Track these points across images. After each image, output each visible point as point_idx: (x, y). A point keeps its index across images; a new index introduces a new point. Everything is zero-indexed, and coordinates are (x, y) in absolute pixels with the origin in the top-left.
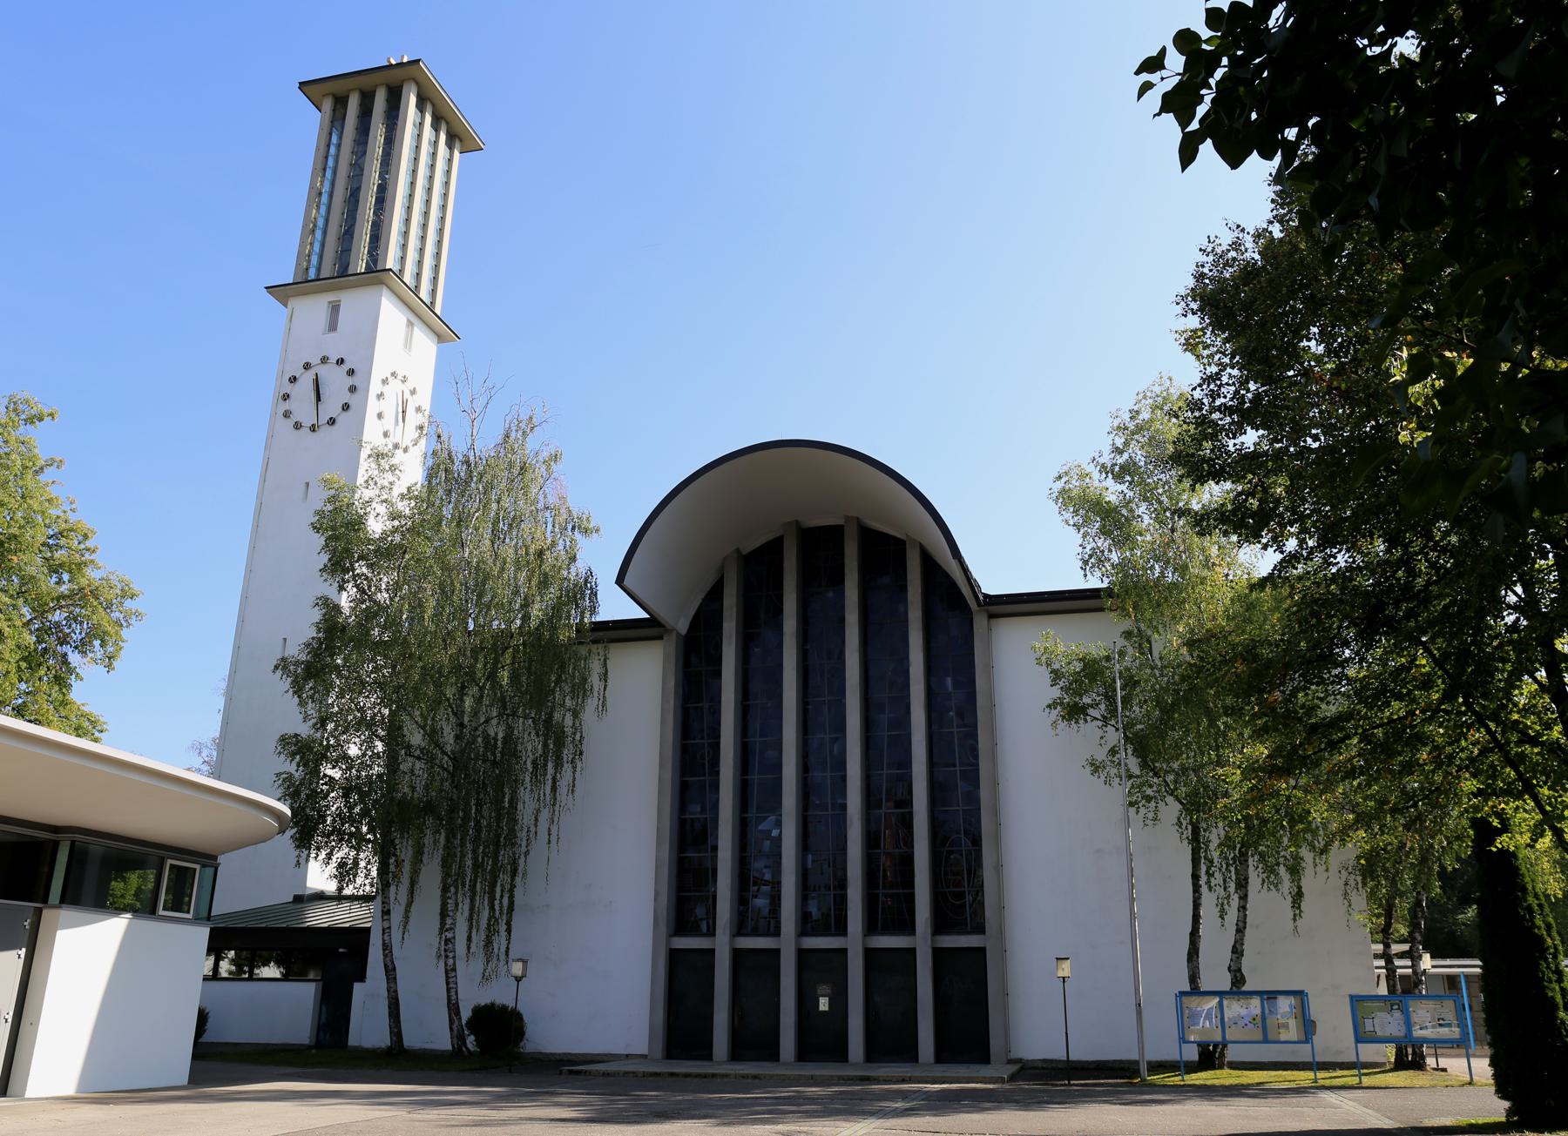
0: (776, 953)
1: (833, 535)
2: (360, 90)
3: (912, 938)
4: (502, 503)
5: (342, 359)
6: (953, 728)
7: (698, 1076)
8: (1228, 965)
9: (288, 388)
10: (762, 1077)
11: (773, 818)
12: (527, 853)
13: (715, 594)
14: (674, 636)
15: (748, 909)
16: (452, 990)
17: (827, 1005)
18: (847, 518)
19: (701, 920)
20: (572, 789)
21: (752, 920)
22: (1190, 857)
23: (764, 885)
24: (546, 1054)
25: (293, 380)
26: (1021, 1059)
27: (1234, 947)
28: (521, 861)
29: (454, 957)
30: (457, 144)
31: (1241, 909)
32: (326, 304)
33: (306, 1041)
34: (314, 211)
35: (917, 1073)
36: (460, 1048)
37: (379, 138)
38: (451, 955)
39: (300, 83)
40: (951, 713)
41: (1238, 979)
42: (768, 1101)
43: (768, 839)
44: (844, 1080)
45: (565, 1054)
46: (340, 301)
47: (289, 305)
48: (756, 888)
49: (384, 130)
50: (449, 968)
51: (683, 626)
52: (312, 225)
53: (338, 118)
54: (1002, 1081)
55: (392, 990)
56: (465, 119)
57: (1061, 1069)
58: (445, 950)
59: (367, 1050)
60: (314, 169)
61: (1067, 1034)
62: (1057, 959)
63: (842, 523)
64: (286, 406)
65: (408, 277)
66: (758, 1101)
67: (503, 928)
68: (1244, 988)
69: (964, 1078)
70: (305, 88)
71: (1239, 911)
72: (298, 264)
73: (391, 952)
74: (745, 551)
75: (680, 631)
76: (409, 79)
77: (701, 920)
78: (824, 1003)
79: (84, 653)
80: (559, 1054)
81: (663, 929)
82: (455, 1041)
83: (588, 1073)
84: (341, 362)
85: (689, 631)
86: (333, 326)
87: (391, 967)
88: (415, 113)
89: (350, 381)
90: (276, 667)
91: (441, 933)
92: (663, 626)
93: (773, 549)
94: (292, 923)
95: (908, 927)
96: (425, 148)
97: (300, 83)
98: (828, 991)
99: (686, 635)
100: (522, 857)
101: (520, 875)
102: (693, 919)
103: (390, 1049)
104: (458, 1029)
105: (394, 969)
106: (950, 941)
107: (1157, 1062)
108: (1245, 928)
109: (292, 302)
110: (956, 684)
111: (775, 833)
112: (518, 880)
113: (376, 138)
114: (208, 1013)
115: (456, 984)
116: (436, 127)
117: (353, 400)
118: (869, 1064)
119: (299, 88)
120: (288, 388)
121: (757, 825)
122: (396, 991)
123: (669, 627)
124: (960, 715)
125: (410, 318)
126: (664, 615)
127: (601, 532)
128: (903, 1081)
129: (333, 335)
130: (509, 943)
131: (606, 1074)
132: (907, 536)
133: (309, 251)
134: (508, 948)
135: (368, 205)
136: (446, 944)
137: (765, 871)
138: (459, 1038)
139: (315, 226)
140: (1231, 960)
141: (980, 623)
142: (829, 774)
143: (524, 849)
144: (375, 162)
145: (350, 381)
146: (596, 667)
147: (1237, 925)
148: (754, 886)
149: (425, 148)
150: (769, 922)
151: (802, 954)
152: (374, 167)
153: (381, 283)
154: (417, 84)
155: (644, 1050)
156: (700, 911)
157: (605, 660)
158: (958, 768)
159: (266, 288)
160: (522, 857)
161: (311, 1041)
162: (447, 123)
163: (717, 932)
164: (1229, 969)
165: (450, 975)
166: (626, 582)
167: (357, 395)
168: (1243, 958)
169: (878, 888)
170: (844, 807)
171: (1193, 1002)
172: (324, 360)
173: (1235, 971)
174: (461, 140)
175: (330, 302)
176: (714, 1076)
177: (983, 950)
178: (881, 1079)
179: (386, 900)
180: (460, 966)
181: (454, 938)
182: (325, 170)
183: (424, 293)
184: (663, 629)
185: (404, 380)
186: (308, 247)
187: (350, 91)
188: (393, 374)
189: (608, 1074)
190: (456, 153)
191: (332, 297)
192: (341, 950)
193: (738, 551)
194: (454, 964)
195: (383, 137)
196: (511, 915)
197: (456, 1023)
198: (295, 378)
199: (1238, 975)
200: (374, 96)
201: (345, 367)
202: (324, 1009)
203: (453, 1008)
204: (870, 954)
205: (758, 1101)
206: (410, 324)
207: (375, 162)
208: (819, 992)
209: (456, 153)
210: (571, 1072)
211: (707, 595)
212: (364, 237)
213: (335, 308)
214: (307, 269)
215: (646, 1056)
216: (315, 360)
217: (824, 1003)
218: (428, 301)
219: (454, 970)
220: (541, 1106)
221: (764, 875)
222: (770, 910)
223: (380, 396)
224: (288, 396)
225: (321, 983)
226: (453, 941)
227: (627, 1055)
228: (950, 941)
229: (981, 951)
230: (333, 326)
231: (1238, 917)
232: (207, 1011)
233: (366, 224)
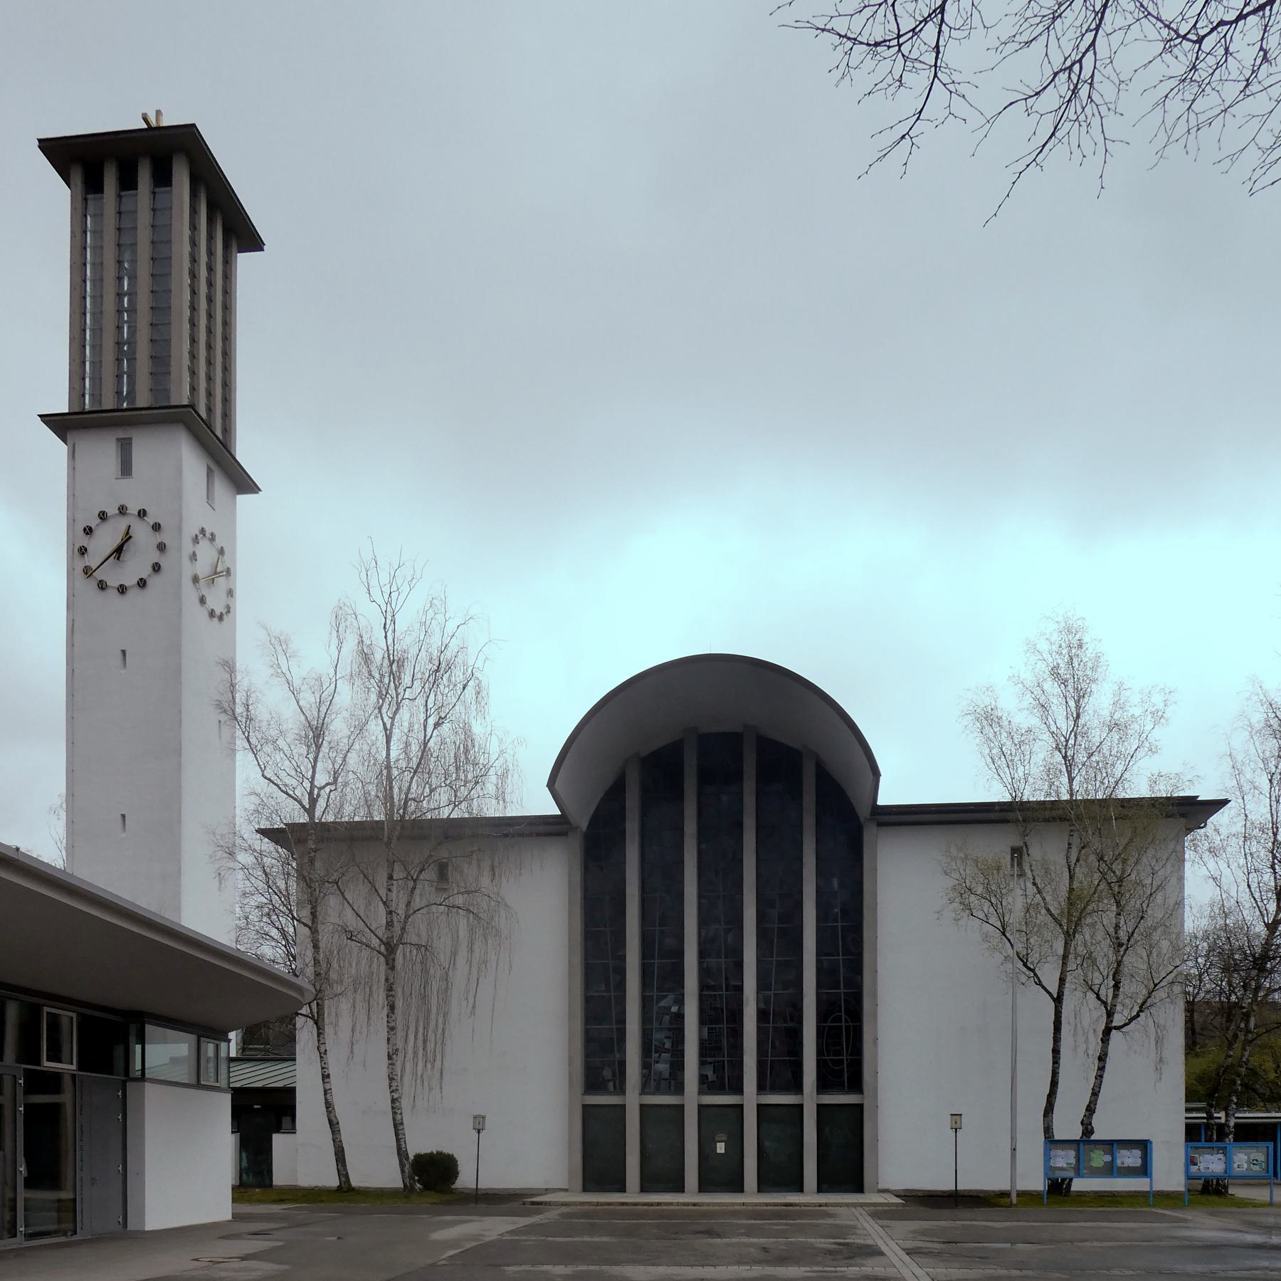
1: (732, 741)
3: (799, 1096)
4: (464, 707)
5: (144, 510)
6: (838, 926)
8: (1081, 1120)
13: (616, 792)
15: (650, 1072)
16: (402, 1140)
17: (723, 1149)
19: (609, 1081)
22: (1052, 1035)
27: (1088, 1106)
29: (401, 1114)
31: (1099, 1078)
38: (399, 1112)
40: (836, 910)
41: (1088, 1129)
43: (667, 1014)
48: (657, 1055)
51: (584, 825)
57: (920, 1196)
59: (305, 1189)
61: (956, 1171)
68: (1093, 1137)
71: (1096, 1078)
74: (643, 755)
77: (609, 1081)
78: (721, 1148)
79: (436, 891)
82: (407, 1181)
87: (335, 1122)
94: (248, 1081)
98: (725, 1138)
102: (600, 1079)
103: (340, 1188)
107: (999, 1191)
108: (1099, 1092)
111: (674, 1009)
118: (585, 1193)
125: (209, 464)
129: (125, 482)
137: (665, 1040)
140: (1085, 1116)
141: (870, 833)
147: (1093, 1089)
148: (655, 1052)
161: (236, 1182)
164: (1082, 1123)
168: (1094, 1115)
170: (740, 989)
171: (481, 1127)
172: (142, 514)
173: (1088, 1124)
179: (326, 1066)
188: (203, 531)
192: (255, 1107)
194: (402, 1119)
198: (90, 529)
199: (1089, 1127)
202: (244, 1155)
206: (210, 472)
211: (605, 795)
217: (721, 1148)
221: (664, 1044)
224: (86, 550)
225: (239, 1134)
229: (860, 1107)
231: (1095, 1084)
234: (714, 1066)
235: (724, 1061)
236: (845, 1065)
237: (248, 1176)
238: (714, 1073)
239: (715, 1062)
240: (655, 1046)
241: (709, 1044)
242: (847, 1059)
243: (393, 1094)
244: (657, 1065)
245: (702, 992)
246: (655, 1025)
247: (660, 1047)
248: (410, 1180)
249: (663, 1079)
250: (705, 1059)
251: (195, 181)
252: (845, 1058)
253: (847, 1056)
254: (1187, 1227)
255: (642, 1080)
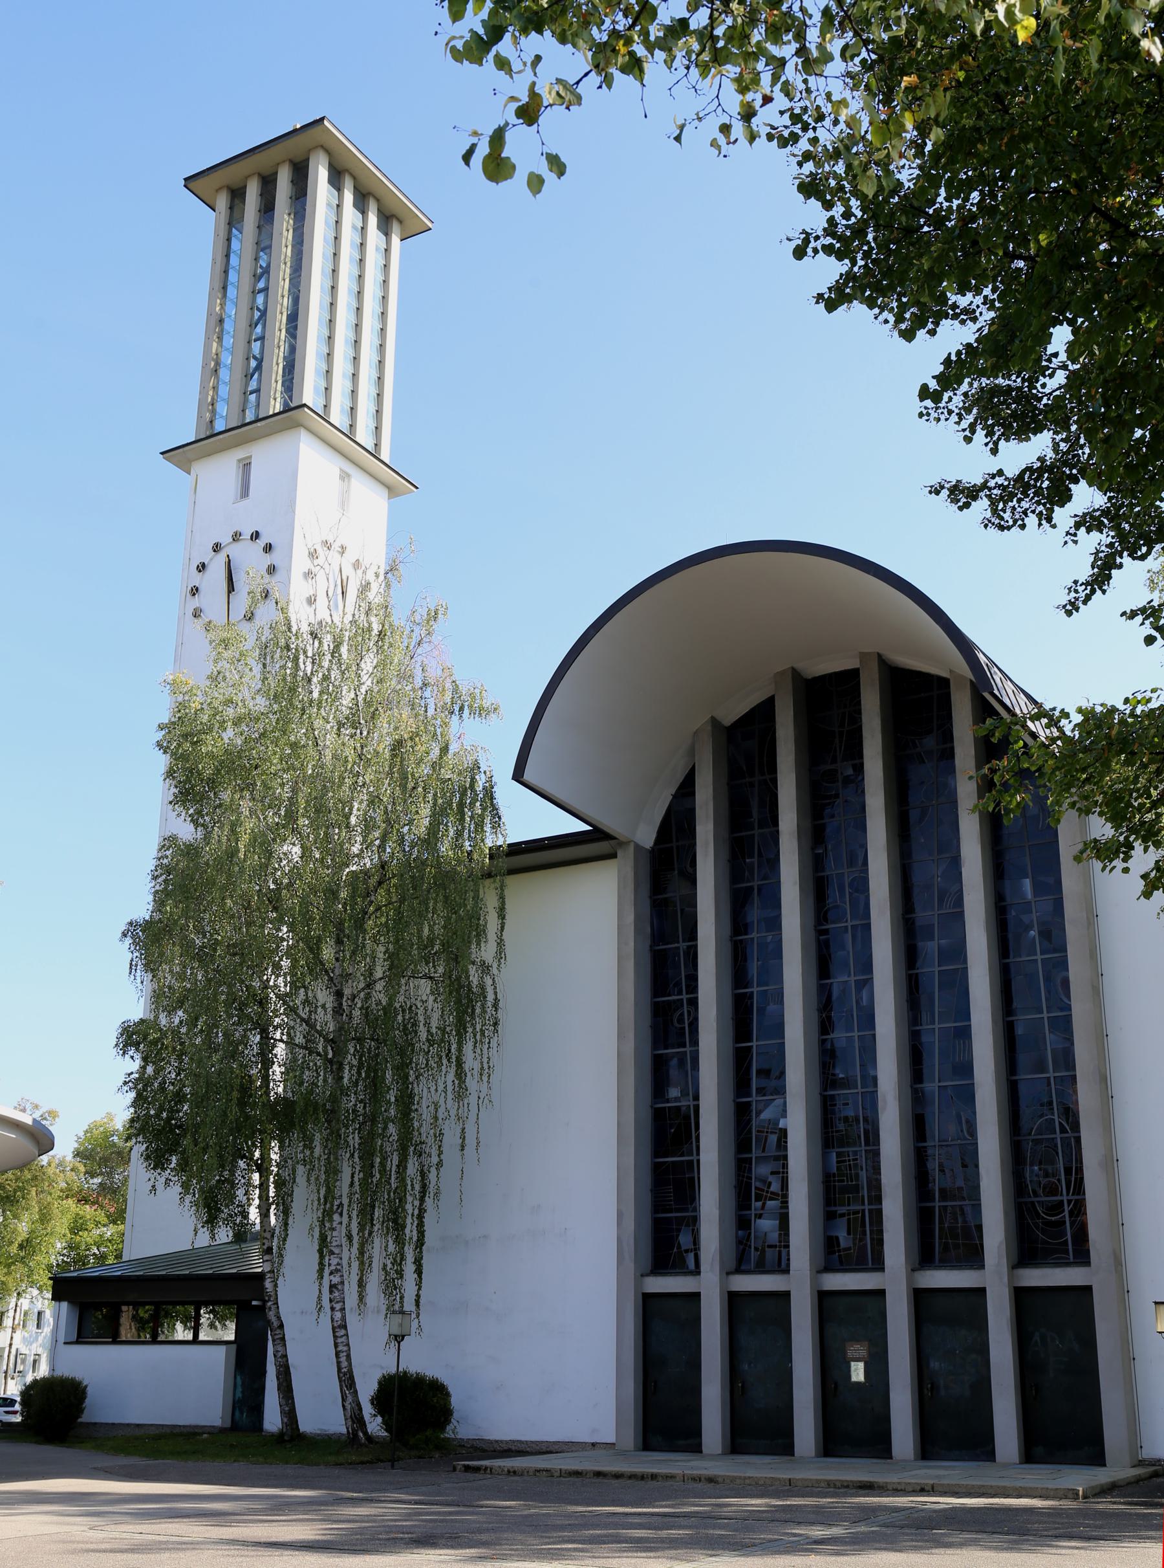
0: (784, 1297)
1: (848, 681)
2: (259, 174)
5: (257, 532)
6: (1036, 954)
7: (633, 1476)
9: (196, 579)
10: (720, 1480)
11: (779, 1102)
12: (440, 1164)
14: (631, 848)
15: (750, 1234)
16: (341, 1355)
17: (853, 1368)
18: (863, 656)
19: (687, 1251)
20: (485, 1071)
21: (756, 1249)
23: (771, 1199)
24: (490, 1442)
25: (202, 567)
26: (1159, 1460)
28: (432, 1176)
29: (343, 1309)
30: (395, 227)
32: (235, 462)
33: (218, 1422)
34: (215, 345)
35: (892, 1478)
36: (355, 1435)
37: (285, 233)
39: (186, 179)
40: (1032, 933)
42: (637, 1520)
44: (835, 1487)
45: (514, 1441)
46: (250, 457)
47: (192, 472)
48: (759, 1204)
49: (291, 222)
50: (335, 1325)
51: (646, 836)
52: (213, 364)
53: (234, 220)
54: (1075, 1495)
55: (280, 1354)
56: (400, 191)
58: (331, 1301)
60: (212, 289)
62: (1156, 1303)
63: (857, 665)
64: (195, 602)
65: (338, 416)
66: (631, 1520)
67: (409, 1268)
69: (1015, 1489)
70: (195, 185)
72: (200, 417)
73: (277, 1303)
74: (729, 718)
75: (641, 843)
76: (316, 147)
77: (687, 1251)
78: (858, 1373)
80: (507, 1442)
81: (630, 1266)
82: (350, 1423)
83: (488, 1471)
84: (256, 536)
85: (658, 841)
86: (245, 492)
88: (329, 191)
89: (267, 560)
90: (124, 935)
91: (321, 1277)
92: (615, 838)
93: (764, 713)
95: (973, 1256)
96: (348, 236)
97: (186, 179)
99: (653, 848)
100: (433, 1170)
101: (432, 1195)
104: (352, 1408)
105: (281, 1326)
106: (1038, 1277)
109: (197, 468)
110: (1038, 888)
112: (429, 1201)
113: (281, 234)
114: (86, 1386)
115: (348, 1345)
116: (361, 204)
117: (273, 583)
119: (185, 186)
120: (196, 579)
121: (758, 1113)
122: (285, 1356)
123: (622, 839)
124: (1046, 934)
126: (609, 823)
127: (502, 710)
128: (922, 1491)
130: (420, 1289)
131: (513, 1472)
132: (951, 671)
133: (213, 399)
134: (418, 1296)
135: (277, 324)
136: (331, 1292)
137: (771, 1178)
138: (356, 1419)
139: (218, 364)
142: (856, 1034)
143: (435, 1160)
144: (283, 266)
145: (267, 560)
146: (491, 901)
148: (756, 1200)
149: (348, 236)
150: (780, 1253)
151: (824, 1298)
152: (281, 274)
153: (297, 425)
154: (328, 152)
155: (611, 1438)
156: (684, 1239)
157: (502, 890)
158: (1045, 1015)
159: (162, 453)
160: (433, 1170)
162: (378, 200)
163: (702, 1268)
165: (337, 1334)
166: (527, 777)
167: (278, 576)
169: (934, 1200)
172: (236, 537)
174: (400, 222)
175: (239, 461)
176: (654, 1477)
177: (1088, 1290)
178: (890, 1487)
180: (352, 1320)
181: (342, 1283)
182: (225, 288)
183: (364, 435)
184: (612, 842)
185: (343, 550)
186: (211, 393)
187: (247, 178)
189: (515, 1472)
190: (395, 239)
191: (240, 453)
192: (254, 1303)
193: (714, 722)
195: (291, 231)
196: (421, 1252)
197: (350, 1399)
198: (203, 565)
200: (276, 180)
201: (261, 543)
202: (238, 1378)
203: (347, 1380)
204: (921, 1298)
205: (631, 1520)
206: (345, 476)
207: (283, 266)
208: (850, 1354)
209: (395, 239)
210: (467, 1469)
212: (275, 368)
213: (246, 466)
214: (211, 422)
215: (614, 1444)
216: (226, 539)
217: (858, 1373)
218: (370, 447)
219: (345, 1327)
220: (308, 1520)
221: (770, 1184)
222: (780, 1235)
223: (309, 575)
224: (197, 589)
225: (234, 1346)
226: (339, 1287)
227: (593, 1445)
228: (1038, 1277)
230: (245, 492)
232: (85, 1383)
233: (276, 351)
234: (849, 1220)
235: (863, 1211)
236: (1066, 1213)
237: (242, 1413)
238: (849, 1233)
239: (849, 1214)
240: (756, 1188)
241: (839, 1181)
242: (1069, 1202)
243: (332, 1277)
244: (758, 1221)
245: (825, 1090)
246: (755, 1153)
247: (763, 1190)
248: (353, 1422)
249: (770, 1246)
250: (833, 1209)
251: (336, 177)
252: (1065, 1199)
253: (1068, 1194)
254: (64, 1542)
255: (737, 1248)
